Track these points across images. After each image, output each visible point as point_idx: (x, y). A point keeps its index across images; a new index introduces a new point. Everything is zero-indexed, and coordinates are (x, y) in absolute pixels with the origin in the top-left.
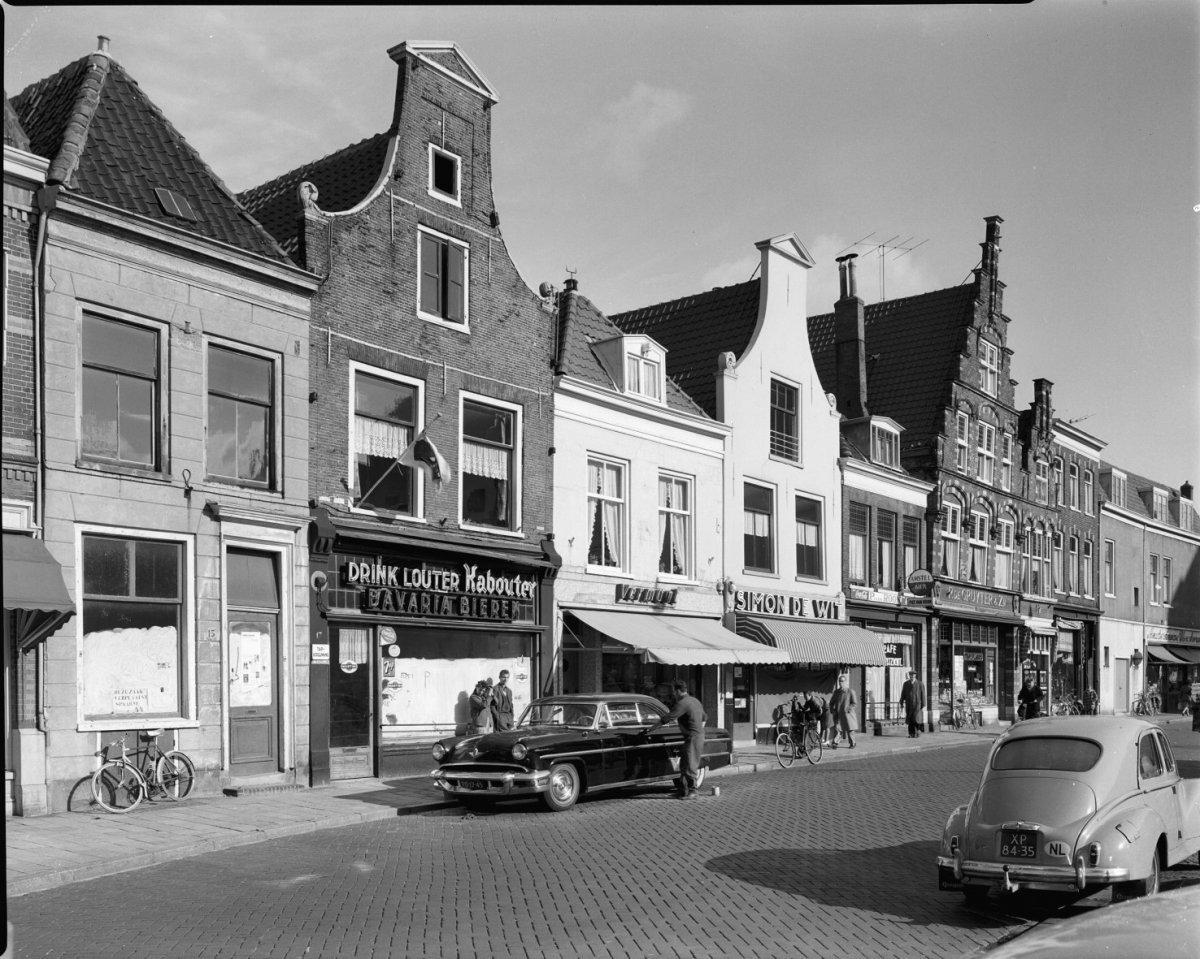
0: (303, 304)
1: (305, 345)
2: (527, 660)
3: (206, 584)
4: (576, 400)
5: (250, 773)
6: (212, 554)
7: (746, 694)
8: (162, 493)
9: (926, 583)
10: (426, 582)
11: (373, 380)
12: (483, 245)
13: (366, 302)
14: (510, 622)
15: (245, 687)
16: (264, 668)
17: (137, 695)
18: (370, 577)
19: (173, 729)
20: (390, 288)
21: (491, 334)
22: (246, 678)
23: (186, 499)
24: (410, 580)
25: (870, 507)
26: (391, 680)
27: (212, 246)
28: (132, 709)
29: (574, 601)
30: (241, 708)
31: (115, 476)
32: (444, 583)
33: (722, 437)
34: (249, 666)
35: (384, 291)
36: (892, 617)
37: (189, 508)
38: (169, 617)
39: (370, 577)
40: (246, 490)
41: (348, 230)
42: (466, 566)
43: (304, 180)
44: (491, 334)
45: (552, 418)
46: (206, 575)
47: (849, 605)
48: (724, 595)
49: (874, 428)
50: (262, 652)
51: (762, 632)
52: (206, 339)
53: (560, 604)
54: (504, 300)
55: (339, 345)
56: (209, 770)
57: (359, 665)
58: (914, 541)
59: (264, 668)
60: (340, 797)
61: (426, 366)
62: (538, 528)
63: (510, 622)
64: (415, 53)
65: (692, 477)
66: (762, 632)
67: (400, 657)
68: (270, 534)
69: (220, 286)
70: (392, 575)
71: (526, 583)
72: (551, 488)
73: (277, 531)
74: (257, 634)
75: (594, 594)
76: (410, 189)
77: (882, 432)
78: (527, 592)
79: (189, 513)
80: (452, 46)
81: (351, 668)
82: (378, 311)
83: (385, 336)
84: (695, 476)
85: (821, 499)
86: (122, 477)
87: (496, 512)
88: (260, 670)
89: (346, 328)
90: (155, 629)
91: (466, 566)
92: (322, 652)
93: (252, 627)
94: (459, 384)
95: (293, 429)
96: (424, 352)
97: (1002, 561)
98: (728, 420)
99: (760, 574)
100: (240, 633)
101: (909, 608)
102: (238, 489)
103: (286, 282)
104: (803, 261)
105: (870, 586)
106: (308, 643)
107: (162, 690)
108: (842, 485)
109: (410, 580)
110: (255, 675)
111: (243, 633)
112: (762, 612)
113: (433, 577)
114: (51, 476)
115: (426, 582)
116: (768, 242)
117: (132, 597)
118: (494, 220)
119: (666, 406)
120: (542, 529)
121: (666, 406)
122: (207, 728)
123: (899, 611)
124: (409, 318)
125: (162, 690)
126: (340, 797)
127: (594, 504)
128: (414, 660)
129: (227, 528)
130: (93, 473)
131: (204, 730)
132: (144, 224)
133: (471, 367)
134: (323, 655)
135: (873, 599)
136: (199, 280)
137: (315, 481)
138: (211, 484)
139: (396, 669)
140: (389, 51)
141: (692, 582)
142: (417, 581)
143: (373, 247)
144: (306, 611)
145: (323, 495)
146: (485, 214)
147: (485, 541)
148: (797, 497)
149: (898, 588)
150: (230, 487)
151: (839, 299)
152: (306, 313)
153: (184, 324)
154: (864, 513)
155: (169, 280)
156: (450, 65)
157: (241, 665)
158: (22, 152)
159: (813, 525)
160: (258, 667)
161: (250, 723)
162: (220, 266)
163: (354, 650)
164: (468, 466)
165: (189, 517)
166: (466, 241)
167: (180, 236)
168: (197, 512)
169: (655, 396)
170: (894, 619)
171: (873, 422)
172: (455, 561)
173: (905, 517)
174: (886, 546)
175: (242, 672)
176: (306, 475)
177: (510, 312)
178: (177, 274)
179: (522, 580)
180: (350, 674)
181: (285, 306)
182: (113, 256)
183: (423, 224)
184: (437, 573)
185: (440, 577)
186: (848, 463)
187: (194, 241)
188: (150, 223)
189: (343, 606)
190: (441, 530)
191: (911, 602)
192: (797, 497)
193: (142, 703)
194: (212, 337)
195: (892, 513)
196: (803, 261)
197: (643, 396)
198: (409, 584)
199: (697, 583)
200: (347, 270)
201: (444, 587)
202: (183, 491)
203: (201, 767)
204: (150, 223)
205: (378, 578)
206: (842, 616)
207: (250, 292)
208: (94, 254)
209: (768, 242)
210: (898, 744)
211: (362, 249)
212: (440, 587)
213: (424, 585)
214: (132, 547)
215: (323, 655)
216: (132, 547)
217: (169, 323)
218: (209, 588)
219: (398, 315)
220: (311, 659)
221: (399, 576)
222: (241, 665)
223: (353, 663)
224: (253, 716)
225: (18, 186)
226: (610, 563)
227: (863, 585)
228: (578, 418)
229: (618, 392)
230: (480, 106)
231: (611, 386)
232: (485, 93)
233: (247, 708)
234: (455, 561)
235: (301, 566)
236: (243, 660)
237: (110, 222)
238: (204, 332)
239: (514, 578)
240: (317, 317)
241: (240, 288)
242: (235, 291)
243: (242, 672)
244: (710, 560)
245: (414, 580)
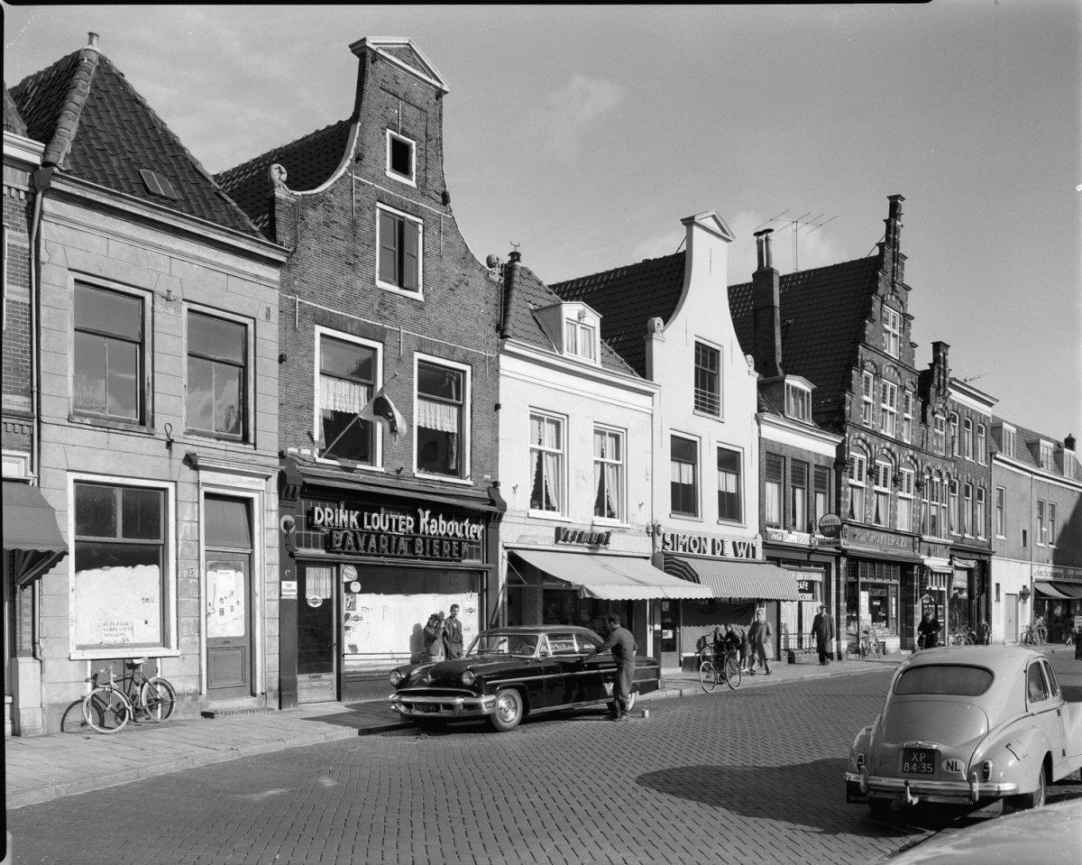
0: (273, 274)
1: (275, 311)
3: (186, 527)
4: (520, 361)
5: (225, 697)
6: (191, 500)
7: (672, 626)
8: (146, 445)
9: (835, 526)
10: (384, 525)
11: (336, 342)
12: (435, 221)
13: (330, 272)
14: (460, 561)
15: (221, 620)
16: (238, 602)
17: (124, 627)
18: (334, 520)
19: (156, 658)
20: (352, 260)
21: (443, 302)
22: (222, 612)
23: (168, 450)
24: (369, 523)
25: (785, 457)
26: (353, 614)
27: (191, 222)
28: (119, 640)
29: (518, 542)
30: (217, 638)
31: (104, 429)
32: (400, 526)
33: (651, 394)
34: (224, 600)
35: (346, 263)
36: (804, 557)
37: (170, 458)
38: (152, 556)
39: (334, 520)
40: (222, 442)
41: (314, 207)
42: (420, 511)
44: (443, 302)
45: (498, 377)
46: (186, 519)
47: (765, 546)
48: (653, 537)
49: (788, 386)
50: (237, 588)
51: (687, 570)
52: (185, 306)
53: (505, 545)
54: (454, 271)
55: (306, 311)
56: (188, 694)
57: (324, 600)
58: (824, 488)
59: (238, 602)
60: (306, 719)
61: (384, 330)
62: (485, 476)
63: (460, 561)
64: (374, 47)
65: (624, 430)
66: (687, 570)
67: (361, 592)
68: (244, 482)
69: (198, 258)
70: (354, 519)
71: (474, 526)
72: (497, 440)
73: (250, 479)
74: (232, 572)
75: (536, 536)
76: (370, 170)
77: (795, 390)
78: (476, 534)
79: (170, 463)
80: (407, 42)
81: (316, 603)
82: (341, 281)
83: (347, 303)
84: (626, 429)
85: (740, 450)
86: (110, 430)
87: (447, 462)
88: (234, 604)
89: (312, 296)
90: (140, 567)
91: (420, 511)
92: (290, 588)
93: (227, 566)
94: (414, 346)
95: (264, 387)
96: (382, 318)
97: (903, 506)
98: (656, 379)
99: (685, 517)
100: (216, 571)
101: (819, 548)
102: (215, 441)
103: (257, 254)
104: (724, 235)
105: (784, 529)
106: (278, 580)
107: (146, 623)
108: (760, 437)
109: (369, 523)
110: (230, 609)
111: (219, 571)
112: (687, 552)
113: (390, 520)
115: (384, 525)
116: (693, 218)
117: (119, 538)
118: (445, 199)
119: (600, 367)
120: (489, 477)
121: (600, 367)
122: (187, 657)
123: (810, 551)
124: (369, 286)
125: (146, 623)
126: (306, 719)
127: (535, 455)
128: (373, 596)
129: (205, 476)
130: (84, 426)
131: (184, 658)
132: (130, 202)
133: (424, 331)
134: (291, 591)
135: (787, 540)
136: (180, 253)
137: (284, 434)
138: (190, 437)
139: (357, 603)
141: (624, 525)
142: (376, 524)
143: (336, 222)
144: (276, 551)
145: (291, 446)
146: (437, 193)
147: (438, 488)
148: (719, 448)
149: (810, 530)
150: (207, 439)
151: (756, 269)
152: (275, 283)
153: (166, 292)
154: (779, 463)
155: (153, 252)
156: (405, 59)
157: (217, 600)
159: (733, 473)
160: (233, 602)
161: (226, 652)
162: (198, 240)
163: (319, 586)
164: (422, 421)
165: (170, 467)
166: (420, 217)
167: (162, 213)
168: (178, 462)
169: (590, 358)
170: (806, 559)
171: (787, 381)
172: (410, 506)
173: (816, 466)
174: (799, 492)
175: (218, 606)
176: (276, 429)
177: (460, 281)
178: (160, 247)
179: (471, 523)
180: (315, 608)
181: (257, 276)
182: (102, 231)
183: (381, 202)
184: (394, 517)
185: (397, 521)
186: (765, 418)
187: (175, 217)
188: (135, 201)
189: (309, 547)
190: (398, 478)
191: (822, 543)
192: (719, 448)
193: (128, 634)
194: (191, 304)
195: (805, 463)
196: (724, 235)
197: (580, 358)
198: (369, 527)
199: (629, 526)
200: (313, 243)
201: (400, 529)
202: (165, 443)
203: (181, 692)
204: (135, 201)
205: (341, 521)
206: (760, 555)
207: (225, 263)
208: (84, 229)
209: (693, 218)
211: (326, 224)
212: (397, 529)
213: (382, 528)
214: (119, 493)
215: (291, 591)
216: (119, 493)
218: (189, 531)
219: (359, 284)
220: (281, 595)
221: (360, 520)
222: (217, 600)
223: (318, 598)
224: (228, 646)
225: (16, 168)
226: (550, 508)
227: (778, 528)
228: (521, 377)
229: (557, 353)
230: (433, 95)
231: (551, 348)
232: (438, 84)
233: (222, 638)
234: (410, 506)
235: (271, 510)
236: (219, 596)
237: (99, 200)
238: (184, 300)
239: (464, 521)
240: (286, 286)
241: (216, 260)
242: (212, 263)
243: (218, 606)
245: (373, 523)
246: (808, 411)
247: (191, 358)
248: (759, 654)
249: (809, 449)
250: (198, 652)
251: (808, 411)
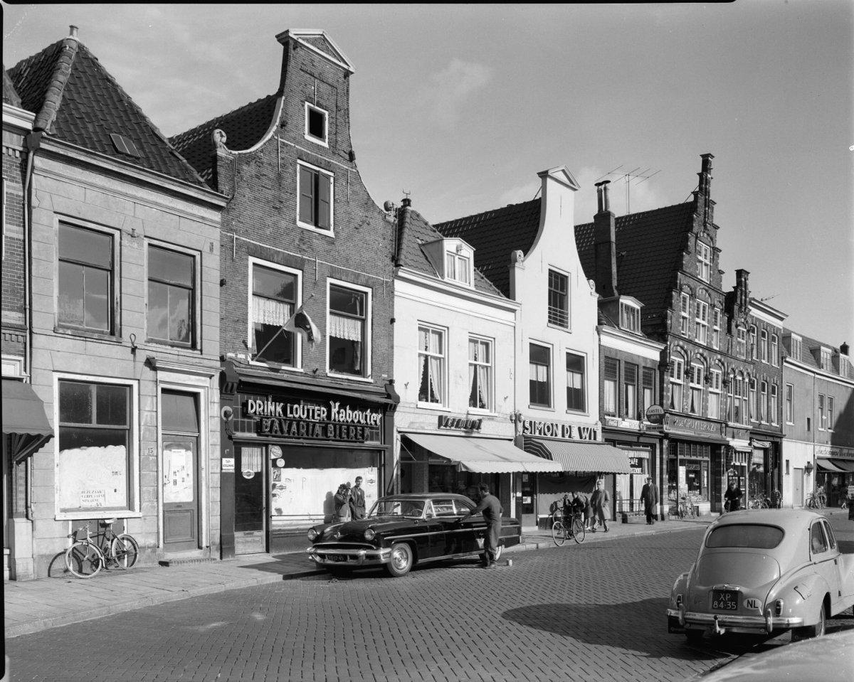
0: (216, 216)
1: (217, 245)
2: (375, 469)
3: (147, 416)
4: (410, 285)
5: (178, 550)
6: (151, 394)
7: (531, 494)
8: (115, 351)
9: (659, 415)
10: (303, 414)
11: (265, 270)
12: (344, 175)
13: (260, 215)
14: (363, 442)
15: (175, 489)
16: (188, 475)
17: (98, 494)
18: (263, 410)
19: (123, 519)
20: (278, 205)
21: (349, 238)
22: (175, 482)
23: (132, 355)
24: (291, 413)
25: (619, 361)
26: (278, 484)
27: (151, 175)
28: (94, 504)
29: (409, 427)
30: (172, 503)
31: (82, 339)
32: (316, 415)
33: (513, 311)
34: (177, 473)
35: (273, 207)
36: (635, 439)
37: (134, 361)
38: (120, 438)
39: (263, 410)
40: (175, 348)
41: (248, 163)
42: (331, 403)
43: (217, 128)
44: (349, 238)
45: (393, 298)
46: (147, 409)
47: (604, 430)
48: (515, 423)
49: (622, 304)
50: (187, 464)
51: (542, 449)
52: (146, 241)
53: (399, 430)
54: (359, 214)
55: (241, 245)
56: (149, 547)
57: (256, 473)
58: (651, 385)
59: (188, 475)
61: (303, 260)
62: (383, 375)
63: (363, 442)
64: (295, 37)
65: (492, 339)
66: (542, 449)
67: (285, 467)
68: (192, 380)
69: (156, 204)
70: (279, 409)
71: (374, 414)
72: (392, 347)
73: (197, 377)
74: (183, 451)
75: (423, 423)
76: (292, 134)
77: (627, 307)
78: (375, 421)
79: (134, 365)
80: (321, 33)
81: (249, 475)
82: (269, 221)
83: (274, 239)
84: (494, 338)
85: (584, 355)
86: (87, 339)
87: (353, 364)
88: (185, 476)
89: (246, 233)
90: (110, 447)
91: (331, 403)
92: (229, 464)
93: (179, 446)
94: (327, 273)
95: (208, 305)
96: (302, 251)
97: (713, 399)
98: (518, 299)
99: (541, 408)
100: (170, 450)
101: (647, 432)
102: (169, 347)
103: (203, 200)
104: (572, 185)
105: (619, 417)
106: (219, 457)
107: (115, 491)
108: (600, 345)
109: (291, 413)
110: (181, 480)
111: (173, 450)
112: (543, 435)
113: (308, 410)
114: (36, 339)
115: (303, 414)
116: (547, 172)
117: (94, 424)
118: (351, 157)
119: (474, 289)
120: (386, 376)
121: (474, 289)
122: (147, 518)
123: (639, 434)
124: (291, 226)
125: (115, 491)
127: (423, 359)
128: (295, 470)
129: (162, 375)
130: (66, 336)
131: (145, 519)
132: (102, 159)
133: (335, 261)
134: (230, 466)
135: (621, 426)
136: (142, 199)
137: (224, 342)
138: (150, 344)
139: (282, 475)
140: (277, 37)
141: (493, 414)
142: (297, 413)
143: (265, 175)
144: (218, 435)
145: (230, 352)
146: (345, 152)
147: (345, 385)
148: (567, 353)
149: (639, 418)
150: (163, 346)
152: (217, 223)
153: (131, 230)
154: (615, 365)
155: (120, 199)
156: (320, 46)
157: (172, 473)
158: (16, 108)
159: (578, 373)
160: (184, 474)
161: (178, 514)
162: (156, 189)
163: (252, 462)
164: (333, 332)
165: (134, 368)
166: (332, 171)
167: (128, 168)
168: (140, 364)
169: (466, 282)
170: (636, 440)
171: (621, 300)
172: (324, 399)
173: (644, 367)
174: (630, 388)
175: (172, 478)
176: (218, 338)
177: (363, 222)
178: (126, 195)
179: (372, 412)
180: (249, 480)
181: (203, 218)
182: (80, 182)
183: (301, 159)
184: (311, 407)
185: (313, 411)
186: (604, 330)
187: (138, 171)
188: (107, 158)
189: (244, 431)
190: (314, 377)
191: (649, 428)
192: (567, 353)
193: (101, 500)
194: (151, 240)
195: (635, 365)
196: (572, 185)
197: (457, 282)
198: (291, 415)
199: (496, 414)
200: (247, 192)
201: (316, 417)
202: (130, 349)
203: (143, 546)
204: (107, 158)
205: (269, 411)
206: (600, 438)
207: (178, 207)
208: (67, 180)
209: (547, 172)
210: (639, 529)
211: (257, 177)
212: (313, 417)
213: (302, 416)
214: (94, 389)
215: (230, 466)
216: (94, 389)
217: (120, 230)
218: (149, 418)
219: (283, 224)
220: (221, 469)
221: (284, 410)
222: (172, 473)
223: (251, 471)
224: (180, 509)
225: (13, 133)
226: (434, 400)
227: (614, 416)
228: (411, 297)
229: (440, 279)
230: (341, 75)
231: (435, 274)
232: (345, 66)
233: (176, 503)
234: (324, 399)
235: (214, 402)
236: (173, 470)
237: (78, 158)
238: (145, 236)
239: (366, 411)
240: (226, 226)
241: (171, 205)
242: (167, 207)
243: (172, 478)
244: (505, 398)
245: (294, 412)
246: (638, 324)
247: (151, 282)
248: (599, 515)
249: (639, 354)
250: (156, 514)
251: (638, 324)
